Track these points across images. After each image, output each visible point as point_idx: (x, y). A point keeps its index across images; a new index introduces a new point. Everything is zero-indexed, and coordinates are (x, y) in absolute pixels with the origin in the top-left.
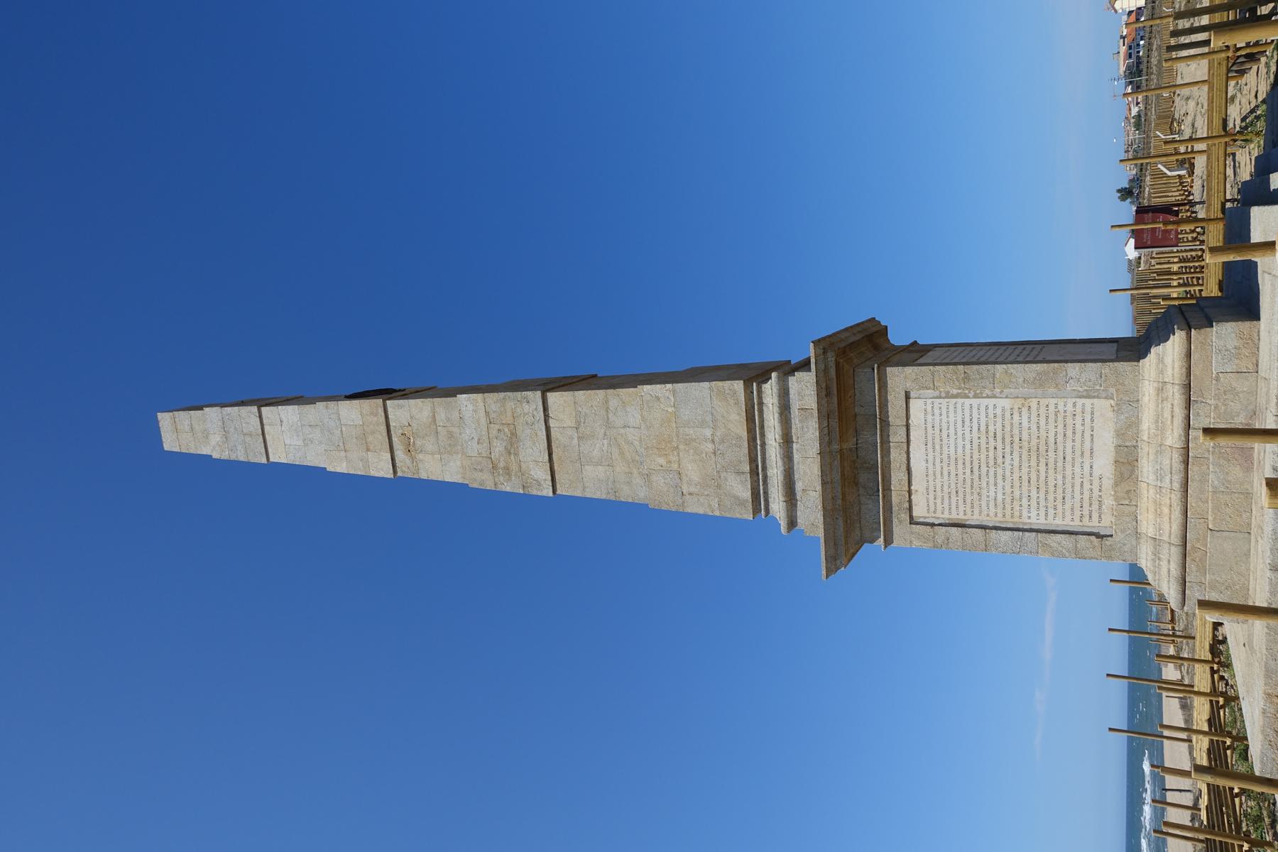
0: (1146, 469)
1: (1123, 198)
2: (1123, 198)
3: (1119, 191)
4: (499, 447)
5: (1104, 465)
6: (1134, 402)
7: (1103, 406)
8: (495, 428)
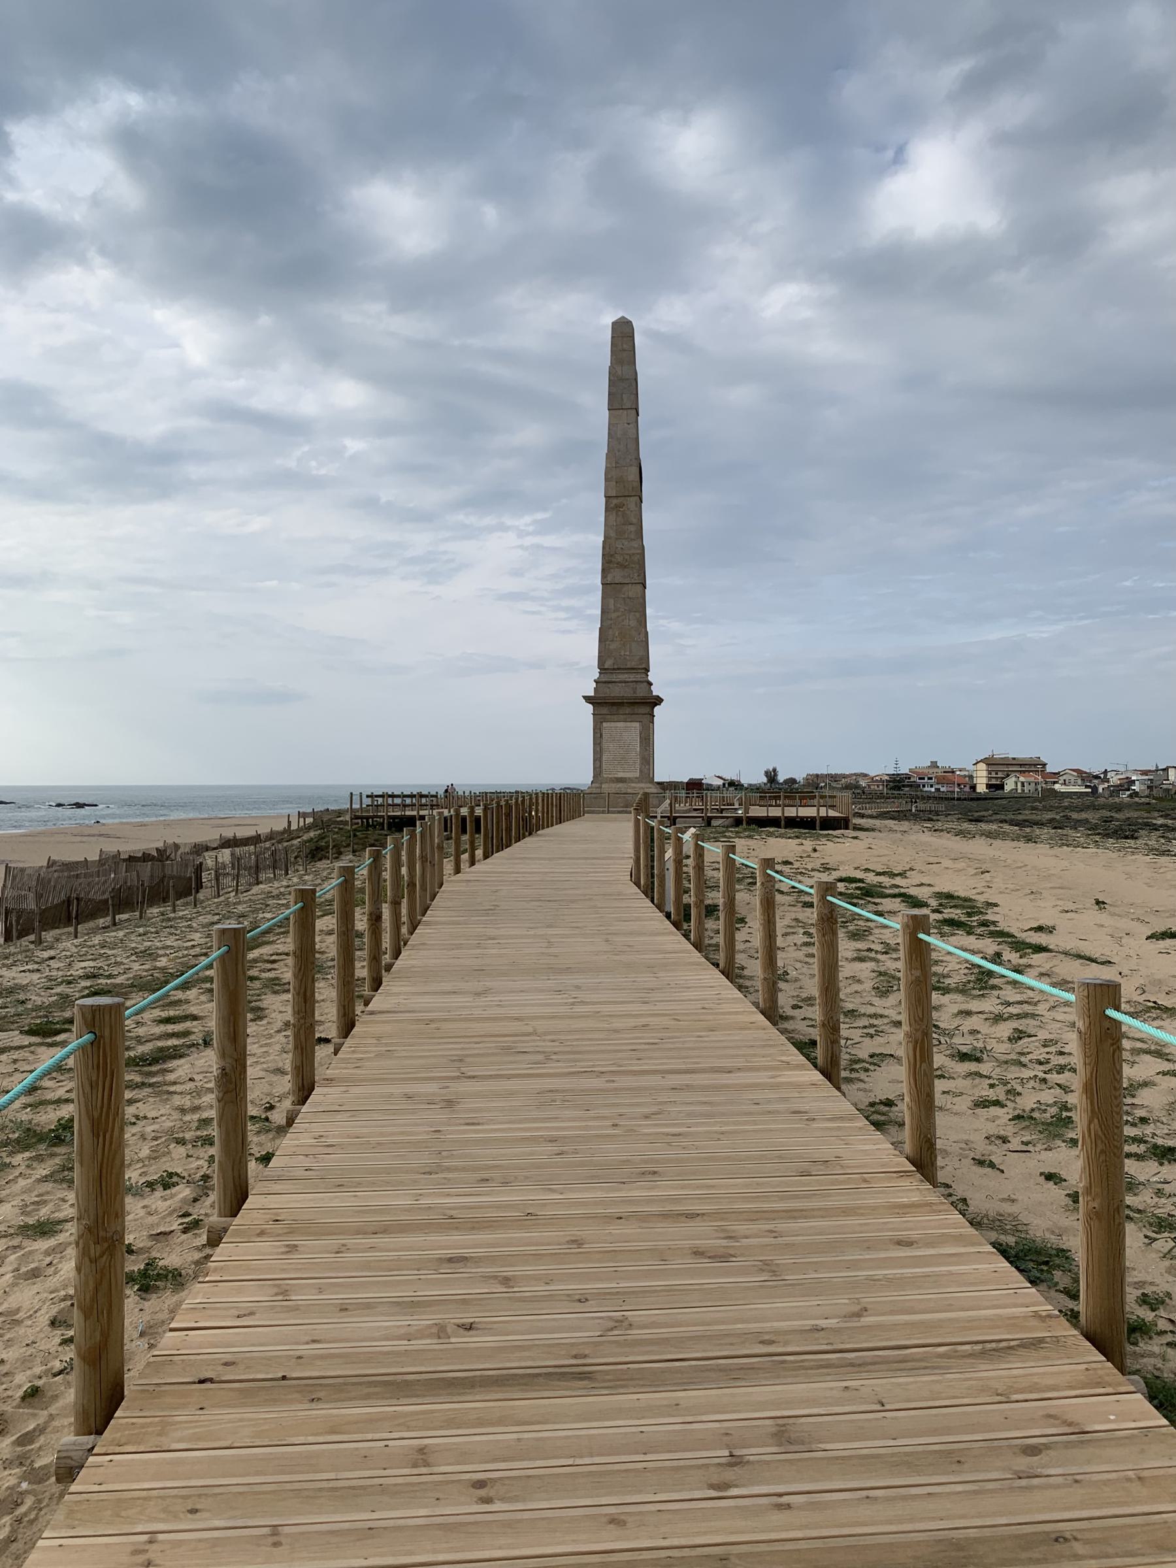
0: (620, 785)
1: (767, 773)
2: (767, 773)
3: (774, 770)
4: (619, 558)
5: (620, 775)
6: (639, 782)
7: (637, 775)
8: (627, 557)
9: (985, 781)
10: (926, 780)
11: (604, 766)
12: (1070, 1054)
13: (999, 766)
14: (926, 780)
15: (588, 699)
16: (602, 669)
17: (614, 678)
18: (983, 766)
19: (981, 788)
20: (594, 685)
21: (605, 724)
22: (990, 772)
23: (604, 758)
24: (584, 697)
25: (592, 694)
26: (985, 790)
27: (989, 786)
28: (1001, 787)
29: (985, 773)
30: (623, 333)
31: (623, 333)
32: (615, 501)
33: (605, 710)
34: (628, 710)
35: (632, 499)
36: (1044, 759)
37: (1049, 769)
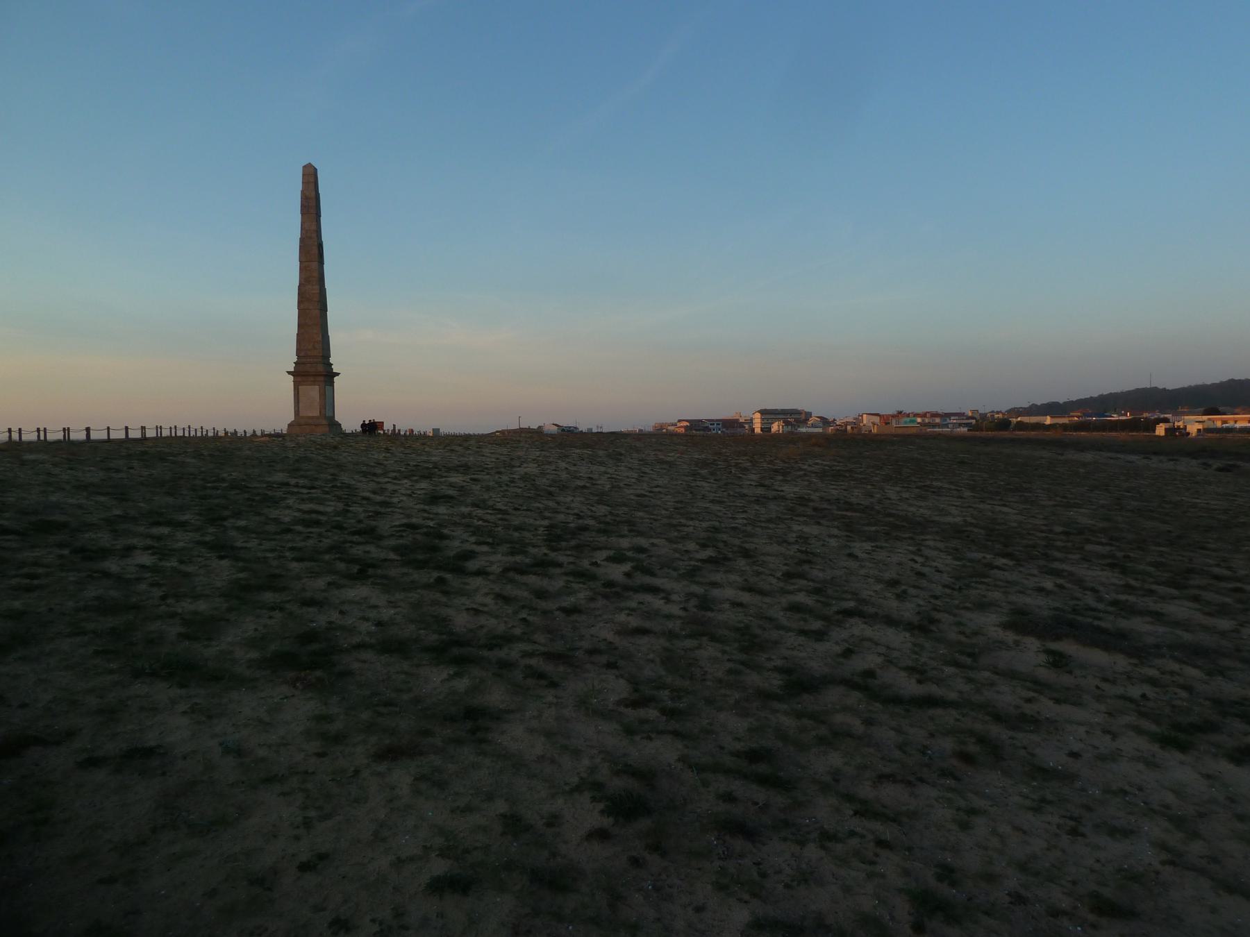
9: (759, 425)
18: (758, 415)
22: (762, 419)
27: (762, 429)
29: (759, 420)
33: (299, 379)
34: (312, 379)
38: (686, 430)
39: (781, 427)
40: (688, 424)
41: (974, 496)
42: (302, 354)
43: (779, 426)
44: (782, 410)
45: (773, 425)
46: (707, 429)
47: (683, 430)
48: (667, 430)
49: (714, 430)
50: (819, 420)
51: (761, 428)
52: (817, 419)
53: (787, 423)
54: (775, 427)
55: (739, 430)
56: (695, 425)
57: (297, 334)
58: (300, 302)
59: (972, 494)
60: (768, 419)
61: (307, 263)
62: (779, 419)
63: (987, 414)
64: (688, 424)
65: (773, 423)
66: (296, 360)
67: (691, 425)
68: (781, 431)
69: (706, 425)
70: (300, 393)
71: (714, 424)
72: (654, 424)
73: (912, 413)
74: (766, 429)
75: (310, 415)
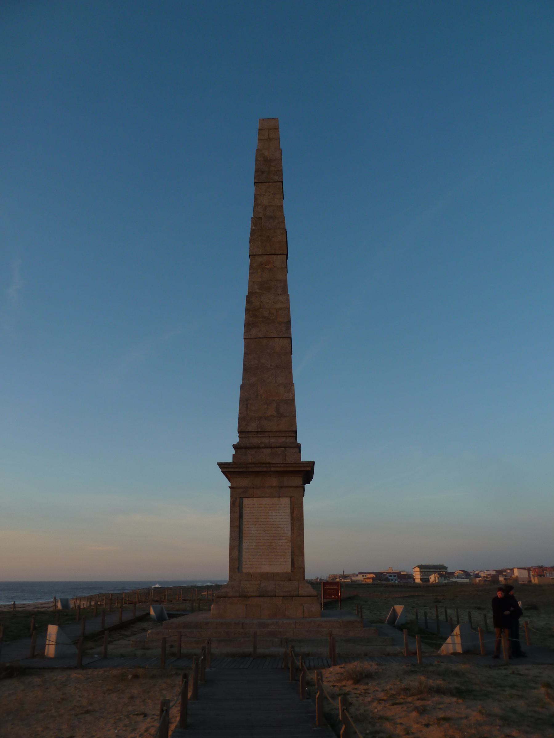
9: (419, 577)
10: (393, 577)
11: (245, 557)
12: (55, 598)
13: (425, 569)
14: (393, 577)
15: (229, 487)
16: (241, 432)
17: (255, 441)
18: (418, 569)
19: (418, 580)
20: (233, 452)
21: (245, 501)
22: (421, 572)
23: (245, 545)
24: (221, 465)
25: (230, 460)
26: (420, 582)
27: (421, 580)
28: (428, 580)
29: (419, 573)
30: (84, 603)
31: (84, 603)
32: (260, 259)
33: (244, 482)
34: (274, 481)
35: (279, 257)
36: (446, 565)
37: (449, 570)
38: (373, 581)
39: (437, 578)
40: (374, 576)
41: (25, 607)
42: (253, 426)
43: (435, 577)
44: (433, 565)
45: (431, 577)
46: (387, 579)
47: (371, 580)
48: (351, 579)
49: (392, 580)
50: (462, 572)
51: (421, 579)
52: (461, 572)
53: (441, 575)
54: (433, 578)
55: (409, 580)
56: (379, 576)
57: (242, 387)
58: (249, 325)
59: (26, 608)
60: (425, 572)
61: (264, 259)
62: (435, 572)
63: (530, 568)
64: (374, 576)
65: (430, 575)
66: (236, 440)
67: (376, 576)
68: (437, 582)
69: (386, 577)
70: (246, 517)
71: (391, 576)
72: (328, 575)
73: (532, 567)
74: (425, 580)
75: (267, 569)
